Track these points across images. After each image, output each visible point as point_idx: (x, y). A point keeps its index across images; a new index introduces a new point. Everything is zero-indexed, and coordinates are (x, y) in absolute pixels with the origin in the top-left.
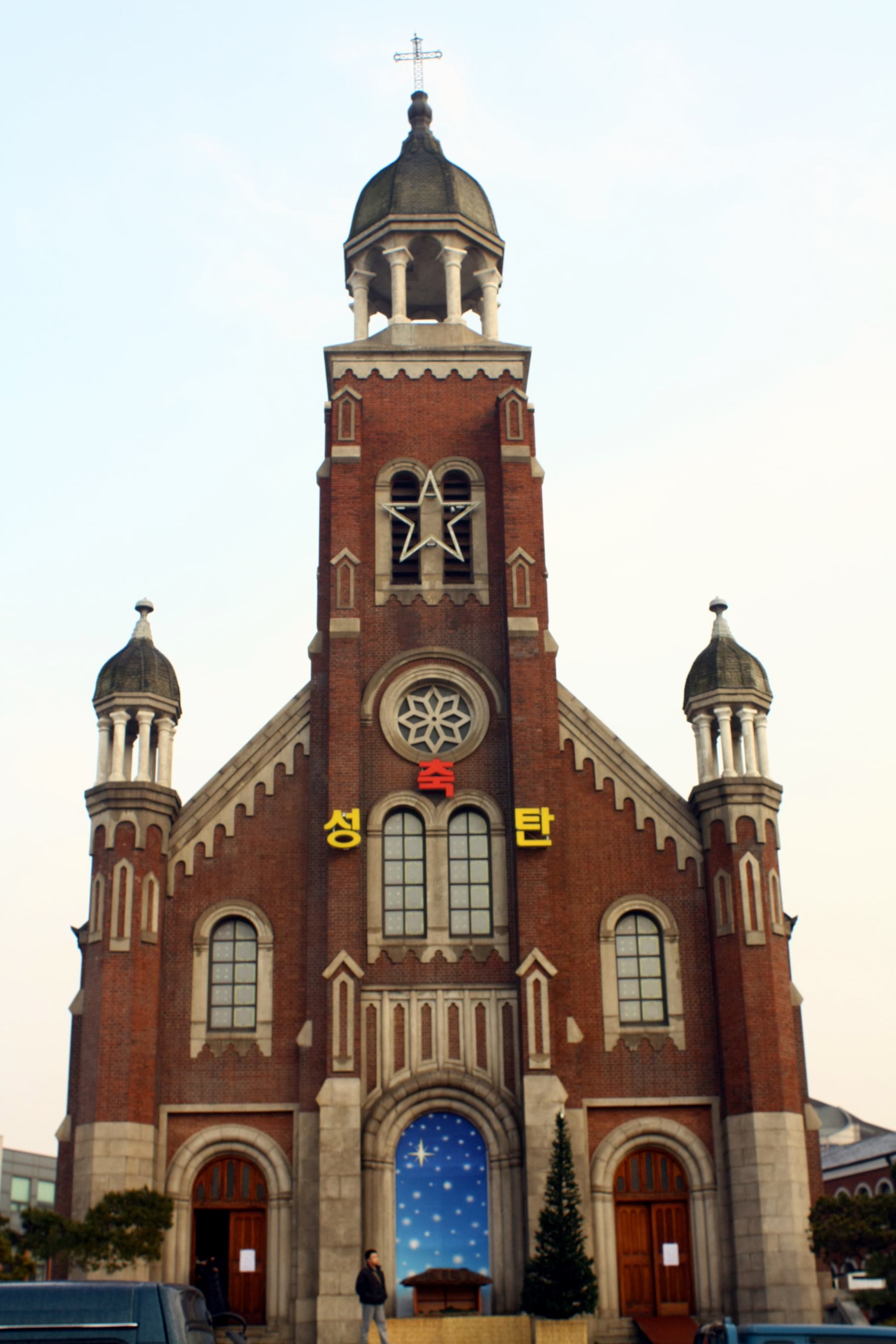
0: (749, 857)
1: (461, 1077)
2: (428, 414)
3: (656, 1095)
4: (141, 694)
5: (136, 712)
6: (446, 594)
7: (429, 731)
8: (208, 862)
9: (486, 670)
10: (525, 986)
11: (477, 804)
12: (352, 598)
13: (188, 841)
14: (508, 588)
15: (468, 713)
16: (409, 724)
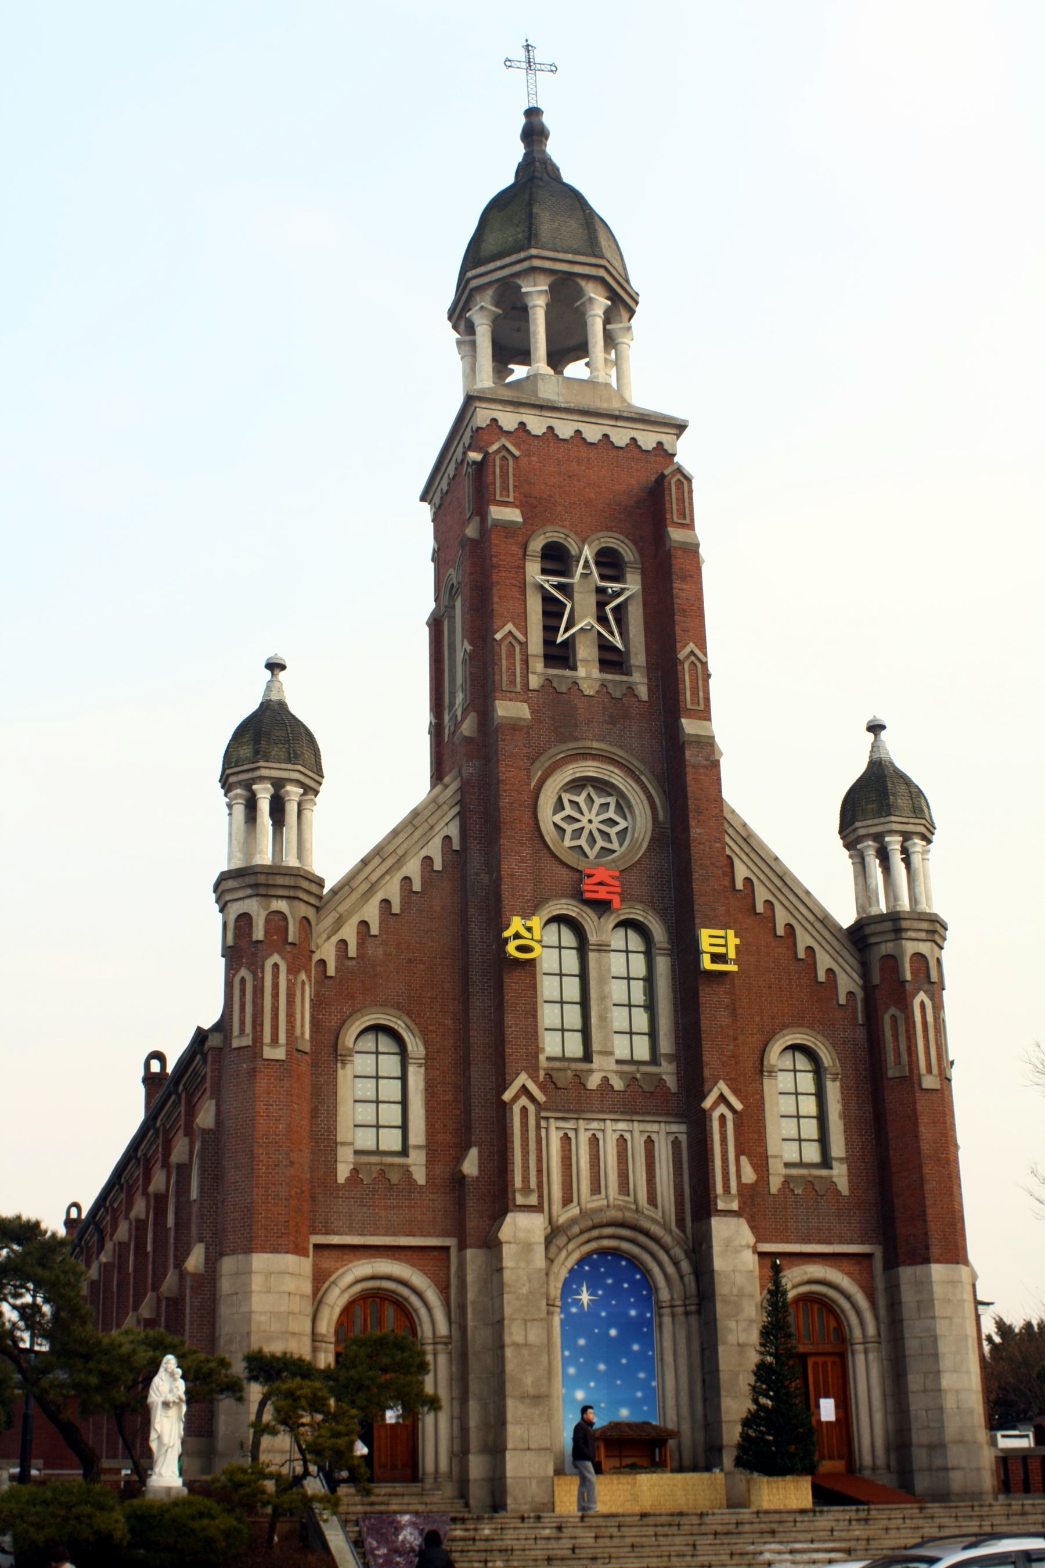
0: (922, 996)
2: (579, 481)
3: (819, 1242)
4: (290, 766)
5: (283, 786)
6: (603, 685)
8: (350, 963)
10: (711, 1120)
11: (641, 919)
13: (329, 938)
14: (681, 686)
16: (564, 825)
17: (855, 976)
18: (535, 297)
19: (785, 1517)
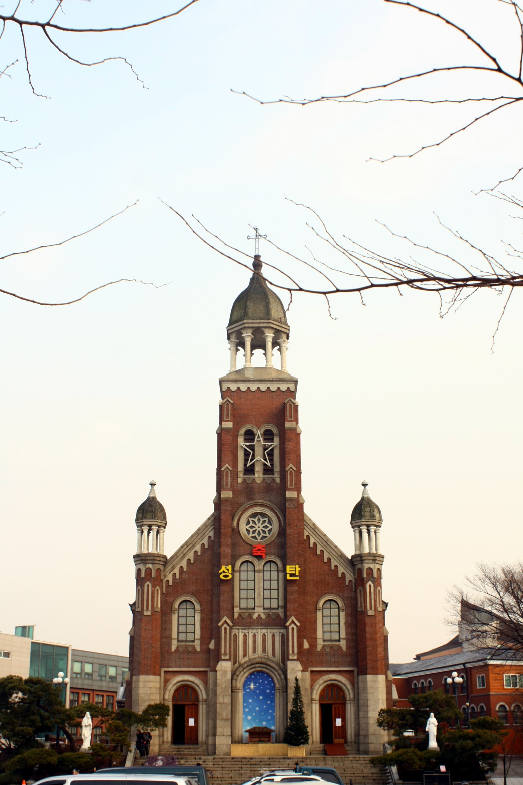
0: (370, 583)
1: (266, 660)
4: (153, 520)
5: (152, 526)
6: (264, 479)
7: (257, 532)
9: (278, 510)
11: (274, 560)
12: (229, 484)
13: (170, 573)
14: (286, 480)
15: (271, 525)
16: (250, 529)
17: (352, 575)
18: (246, 338)
19: (276, 760)
